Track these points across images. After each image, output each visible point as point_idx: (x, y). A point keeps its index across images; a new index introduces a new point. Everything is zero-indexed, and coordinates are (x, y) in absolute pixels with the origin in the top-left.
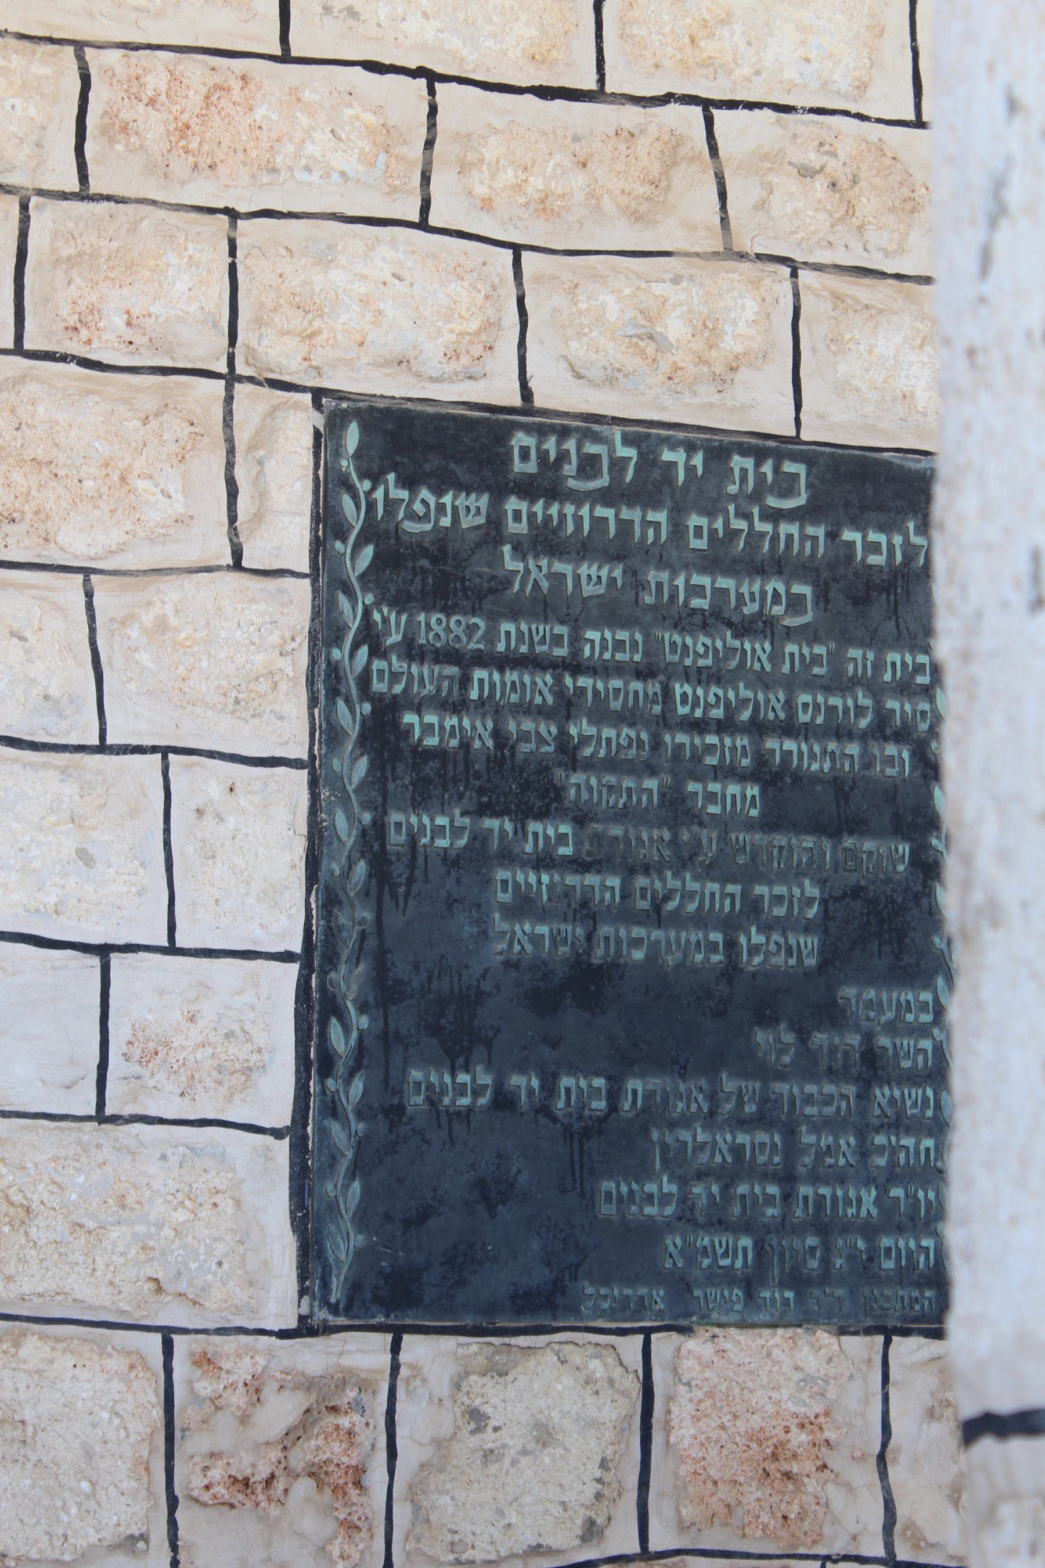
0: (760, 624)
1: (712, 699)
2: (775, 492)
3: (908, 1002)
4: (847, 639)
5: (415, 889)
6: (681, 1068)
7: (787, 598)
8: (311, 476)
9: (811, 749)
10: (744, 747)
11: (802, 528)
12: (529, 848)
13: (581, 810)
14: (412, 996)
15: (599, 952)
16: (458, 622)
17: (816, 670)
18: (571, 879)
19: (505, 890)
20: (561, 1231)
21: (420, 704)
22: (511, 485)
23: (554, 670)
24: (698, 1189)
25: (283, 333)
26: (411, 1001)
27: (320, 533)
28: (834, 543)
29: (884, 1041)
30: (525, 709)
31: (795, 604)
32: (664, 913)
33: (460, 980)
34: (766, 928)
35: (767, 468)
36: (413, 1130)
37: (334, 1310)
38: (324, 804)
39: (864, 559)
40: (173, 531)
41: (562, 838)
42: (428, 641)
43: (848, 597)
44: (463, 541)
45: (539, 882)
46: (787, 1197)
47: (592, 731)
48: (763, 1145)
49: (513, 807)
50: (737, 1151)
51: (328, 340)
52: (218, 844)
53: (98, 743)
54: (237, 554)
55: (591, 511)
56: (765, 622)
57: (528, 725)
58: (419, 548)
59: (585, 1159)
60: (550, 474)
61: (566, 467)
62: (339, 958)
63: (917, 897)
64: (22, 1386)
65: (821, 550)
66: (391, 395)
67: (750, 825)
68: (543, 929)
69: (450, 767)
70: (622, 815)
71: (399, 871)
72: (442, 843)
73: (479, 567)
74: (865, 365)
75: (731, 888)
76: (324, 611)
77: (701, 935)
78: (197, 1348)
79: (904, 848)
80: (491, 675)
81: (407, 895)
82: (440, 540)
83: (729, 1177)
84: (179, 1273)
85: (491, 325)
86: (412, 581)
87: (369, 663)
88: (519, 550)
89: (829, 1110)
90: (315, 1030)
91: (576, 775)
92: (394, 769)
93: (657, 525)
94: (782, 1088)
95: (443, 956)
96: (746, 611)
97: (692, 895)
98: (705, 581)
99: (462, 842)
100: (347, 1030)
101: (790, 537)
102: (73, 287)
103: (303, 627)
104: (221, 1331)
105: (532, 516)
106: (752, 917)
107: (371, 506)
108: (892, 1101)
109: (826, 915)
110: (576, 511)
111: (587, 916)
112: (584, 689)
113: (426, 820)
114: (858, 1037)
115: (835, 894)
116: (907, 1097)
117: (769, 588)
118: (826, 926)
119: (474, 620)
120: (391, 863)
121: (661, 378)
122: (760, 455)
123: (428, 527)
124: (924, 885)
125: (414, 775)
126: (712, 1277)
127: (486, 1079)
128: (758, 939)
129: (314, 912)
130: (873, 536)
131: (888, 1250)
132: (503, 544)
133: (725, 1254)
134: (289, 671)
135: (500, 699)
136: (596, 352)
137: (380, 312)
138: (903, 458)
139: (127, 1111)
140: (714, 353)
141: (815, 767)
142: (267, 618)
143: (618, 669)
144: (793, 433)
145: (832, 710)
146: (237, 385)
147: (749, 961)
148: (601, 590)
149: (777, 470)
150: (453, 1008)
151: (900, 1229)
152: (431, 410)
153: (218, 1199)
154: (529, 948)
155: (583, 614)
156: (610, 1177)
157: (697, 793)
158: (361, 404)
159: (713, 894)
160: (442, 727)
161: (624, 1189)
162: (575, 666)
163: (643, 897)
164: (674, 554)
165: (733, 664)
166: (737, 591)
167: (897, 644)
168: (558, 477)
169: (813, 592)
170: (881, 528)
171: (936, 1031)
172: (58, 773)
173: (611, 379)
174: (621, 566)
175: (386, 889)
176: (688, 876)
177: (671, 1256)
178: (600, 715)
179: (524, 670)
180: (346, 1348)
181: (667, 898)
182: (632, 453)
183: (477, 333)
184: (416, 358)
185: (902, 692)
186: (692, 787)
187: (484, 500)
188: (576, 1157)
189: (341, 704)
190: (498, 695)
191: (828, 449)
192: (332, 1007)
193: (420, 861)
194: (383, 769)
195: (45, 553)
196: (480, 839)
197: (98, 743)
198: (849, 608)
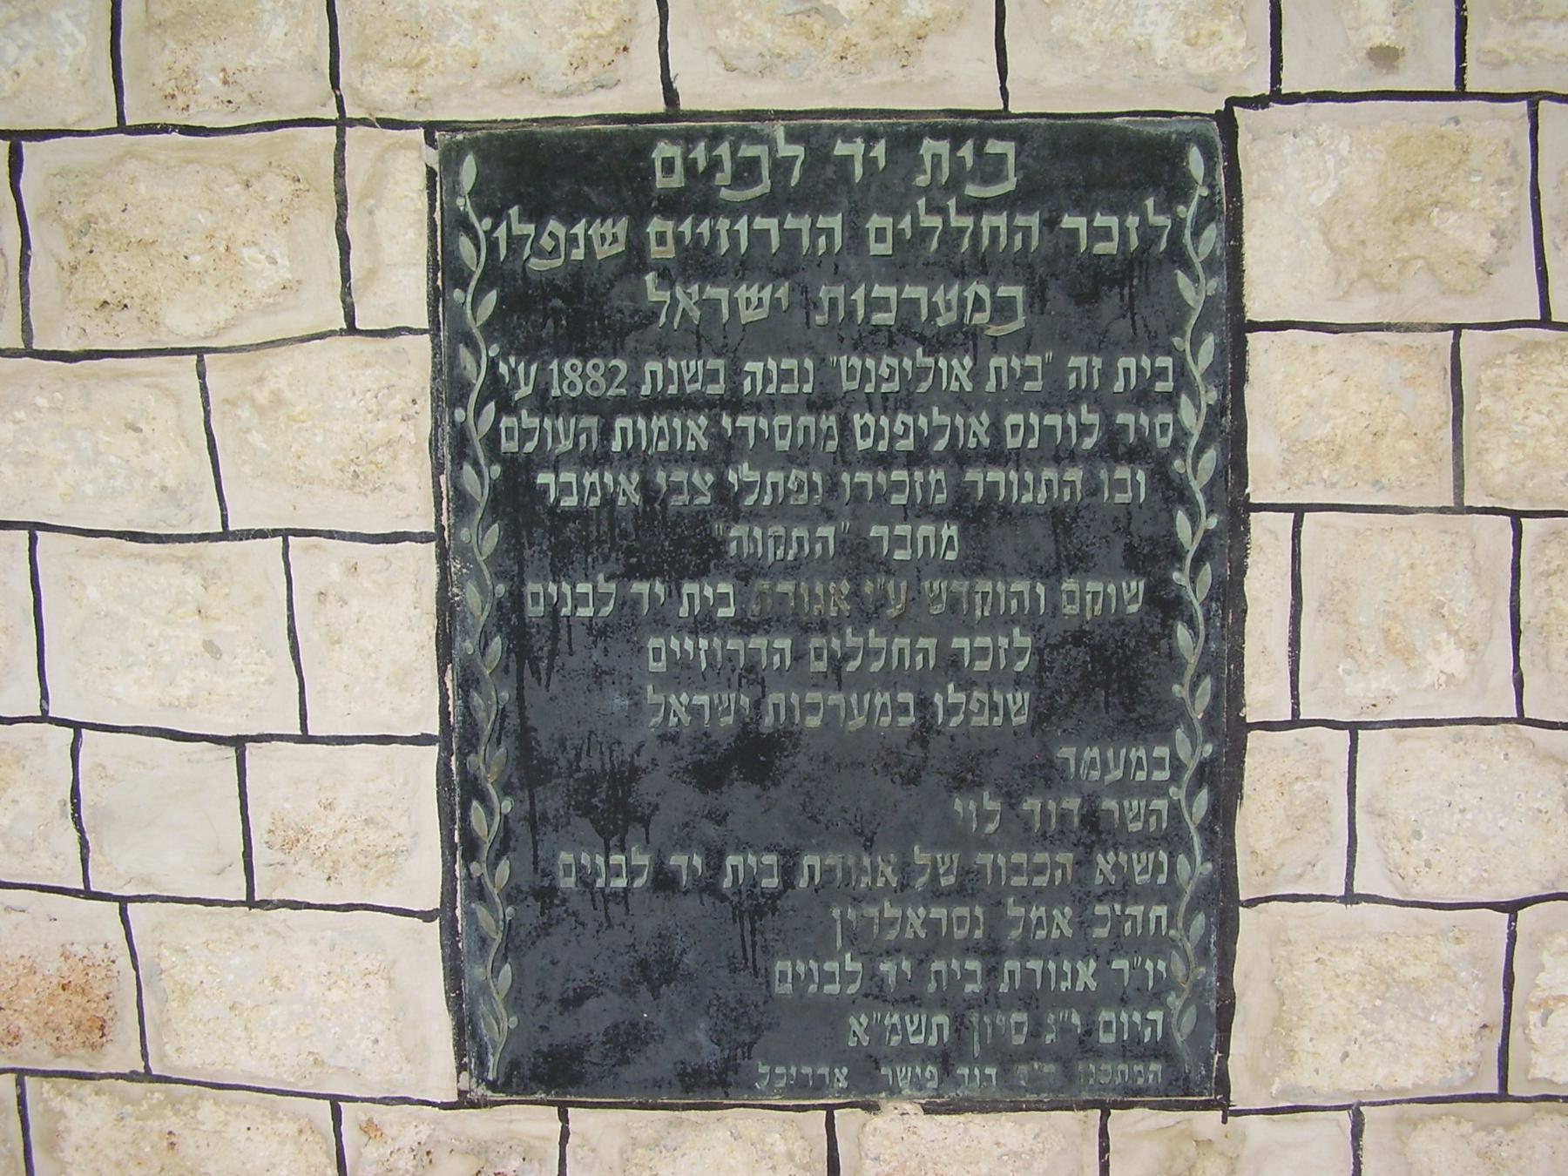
0: (960, 336)
1: (898, 428)
2: (978, 179)
3: (1139, 758)
4: (1066, 342)
5: (558, 661)
6: (867, 840)
7: (993, 303)
8: (425, 221)
9: (1021, 480)
10: (938, 481)
11: (1010, 218)
12: (684, 611)
13: (744, 565)
14: (559, 775)
15: (768, 720)
16: (595, 367)
17: (1028, 386)
18: (734, 644)
19: (657, 659)
20: (732, 1010)
21: (557, 460)
22: (654, 204)
23: (710, 410)
24: (886, 967)
25: (391, 65)
26: (559, 781)
27: (439, 283)
28: (1051, 231)
29: (1110, 804)
30: (676, 457)
31: (1003, 309)
32: (844, 675)
33: (611, 756)
34: (966, 685)
35: (967, 151)
36: (566, 911)
37: (492, 1086)
38: (454, 577)
39: (1089, 248)
40: (281, 299)
41: (722, 599)
42: (562, 391)
43: (1070, 295)
44: (600, 274)
45: (697, 648)
46: (992, 972)
47: (755, 476)
48: (961, 920)
49: (666, 567)
50: (932, 925)
51: (436, 66)
52: (343, 628)
53: (221, 530)
54: (350, 317)
55: (750, 224)
56: (965, 334)
57: (679, 475)
58: (549, 286)
59: (758, 937)
60: (701, 186)
61: (718, 175)
62: (478, 739)
63: (1153, 640)
64: (203, 1144)
65: (1035, 243)
66: (513, 118)
67: (947, 570)
68: (702, 699)
69: (593, 528)
70: (792, 569)
71: (541, 644)
72: (586, 612)
73: (619, 299)
74: (1088, 15)
75: (923, 642)
76: (445, 369)
77: (887, 696)
78: (363, 1118)
79: (1138, 586)
80: (635, 423)
81: (550, 668)
82: (573, 276)
83: (923, 954)
84: (338, 1048)
85: (627, 23)
86: (544, 325)
87: (497, 420)
88: (666, 276)
89: (1041, 881)
90: (458, 813)
91: (737, 526)
92: (530, 534)
93: (829, 233)
94: (985, 859)
95: (591, 732)
96: (940, 322)
97: (877, 652)
98: (890, 292)
99: (607, 610)
100: (490, 812)
101: (995, 231)
102: (167, 52)
103: (423, 389)
104: (386, 1101)
105: (679, 238)
106: (950, 673)
107: (493, 246)
108: (1117, 867)
109: (1042, 667)
110: (732, 225)
111: (755, 680)
112: (744, 430)
113: (566, 588)
114: (1078, 801)
115: (1052, 641)
116: (1135, 862)
117: (969, 295)
118: (1041, 678)
119: (614, 362)
120: (531, 636)
121: (829, 59)
122: (956, 136)
123: (558, 262)
124: (1164, 625)
125: (553, 539)
126: (906, 1054)
127: (642, 860)
128: (956, 697)
129: (450, 693)
130: (1100, 220)
131: (1108, 1024)
132: (647, 272)
133: (917, 1032)
134: (411, 437)
135: (648, 448)
136: (750, 38)
137: (494, 27)
138: (1141, 123)
139: (276, 896)
140: (896, 22)
141: (1027, 498)
142: (384, 383)
143: (788, 403)
144: (1001, 107)
145: (1048, 431)
146: (348, 129)
147: (946, 723)
148: (762, 314)
149: (979, 151)
150: (605, 785)
151: (1123, 1002)
152: (559, 129)
153: (369, 979)
154: (686, 719)
155: (743, 343)
156: (786, 956)
157: (881, 538)
158: (479, 133)
159: (901, 651)
160: (580, 485)
161: (801, 968)
162: (735, 403)
163: (819, 657)
164: (853, 262)
165: (924, 387)
166: (929, 299)
167: (1132, 348)
168: (710, 188)
169: (1027, 294)
170: (1112, 210)
171: (1172, 790)
172: (180, 565)
173: (768, 65)
174: (787, 284)
175: (527, 665)
176: (872, 632)
177: (855, 1034)
178: (764, 455)
179: (675, 413)
180: (513, 1117)
181: (847, 657)
182: (798, 151)
183: (610, 35)
184: (537, 73)
185: (1138, 402)
186: (876, 531)
187: (622, 226)
188: (748, 938)
189: (468, 468)
190: (644, 444)
191: (1043, 121)
192: (472, 789)
193: (563, 632)
194: (517, 535)
195: (155, 337)
196: (627, 604)
197: (221, 530)
198: (1072, 308)
